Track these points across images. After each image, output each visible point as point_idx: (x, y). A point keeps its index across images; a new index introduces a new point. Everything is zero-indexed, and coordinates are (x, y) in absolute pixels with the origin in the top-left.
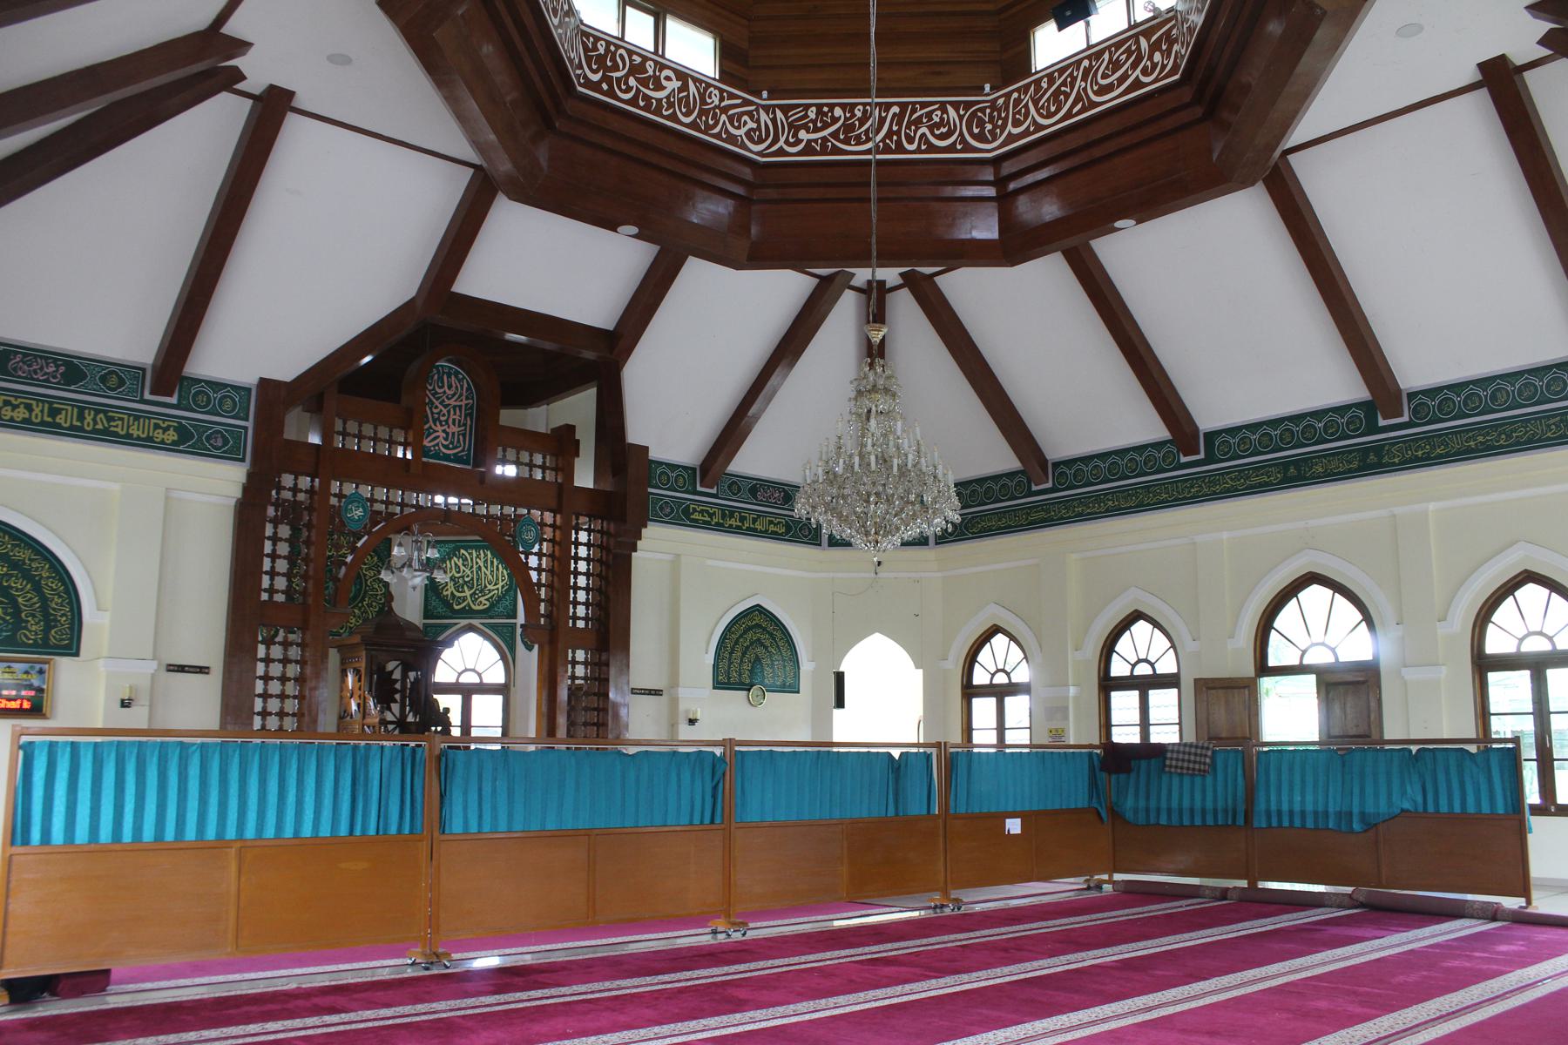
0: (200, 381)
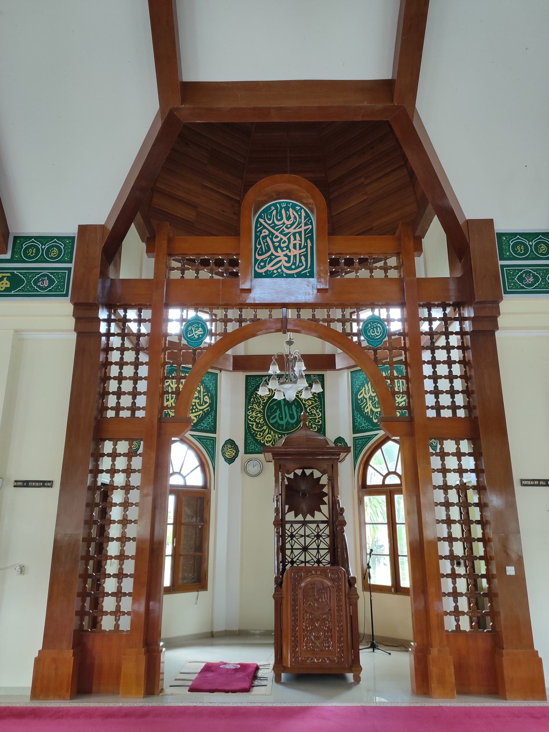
0: (30, 238)
